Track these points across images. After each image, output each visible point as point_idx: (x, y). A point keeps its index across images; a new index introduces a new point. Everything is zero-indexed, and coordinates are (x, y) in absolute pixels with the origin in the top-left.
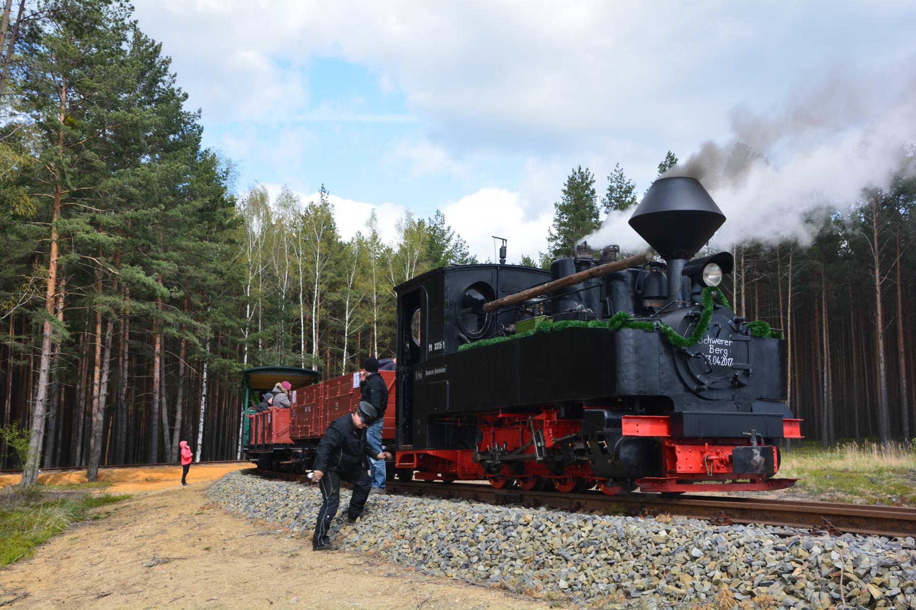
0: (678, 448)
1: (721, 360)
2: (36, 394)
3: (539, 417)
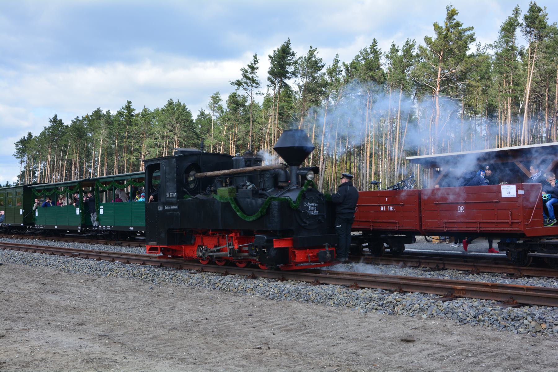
0: (297, 252)
1: (313, 212)
2: (467, 272)
3: (231, 235)
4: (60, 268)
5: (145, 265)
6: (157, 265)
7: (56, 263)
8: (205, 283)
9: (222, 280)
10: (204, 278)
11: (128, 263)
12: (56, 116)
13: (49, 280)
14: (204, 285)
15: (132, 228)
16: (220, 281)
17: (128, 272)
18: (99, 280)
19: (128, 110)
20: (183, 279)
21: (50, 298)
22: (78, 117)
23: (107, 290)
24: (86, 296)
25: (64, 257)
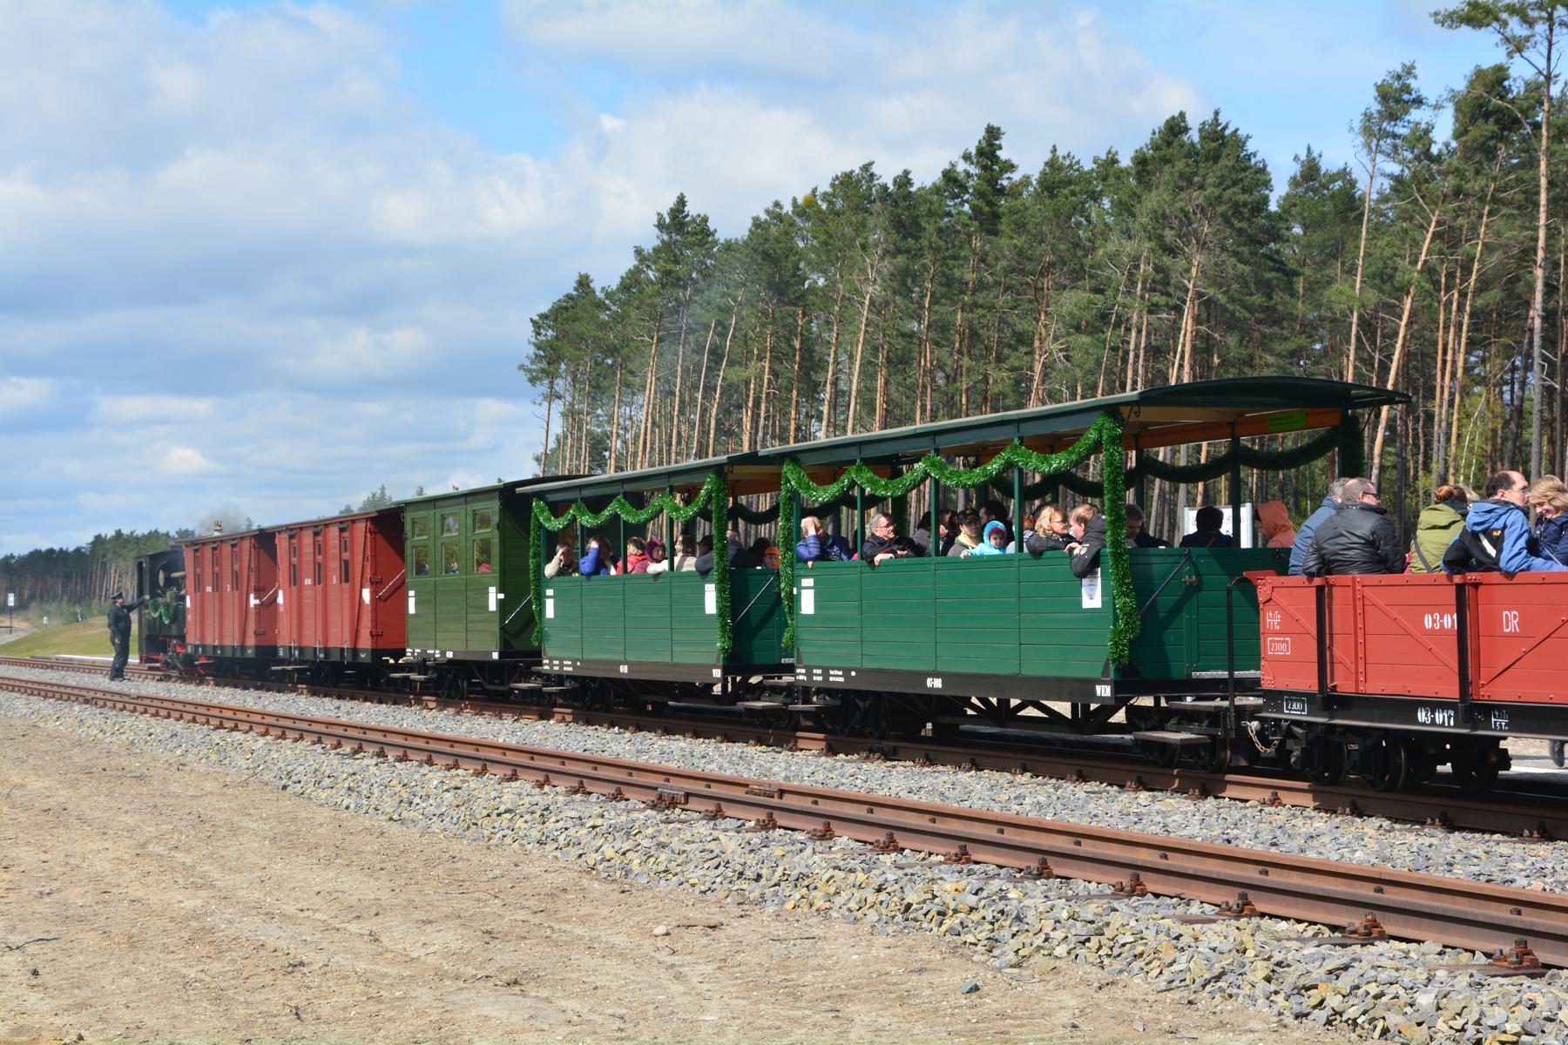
4: (592, 858)
5: (968, 861)
6: (1023, 865)
7: (584, 831)
8: (1250, 977)
9: (1346, 968)
10: (1250, 953)
11: (890, 846)
12: (681, 202)
13: (522, 915)
14: (1247, 990)
15: (937, 683)
16: (1334, 973)
17: (883, 896)
18: (737, 928)
19: (985, 168)
20: (1139, 949)
21: (485, 1011)
22: (777, 204)
23: (757, 987)
24: (651, 1014)
25: (622, 804)
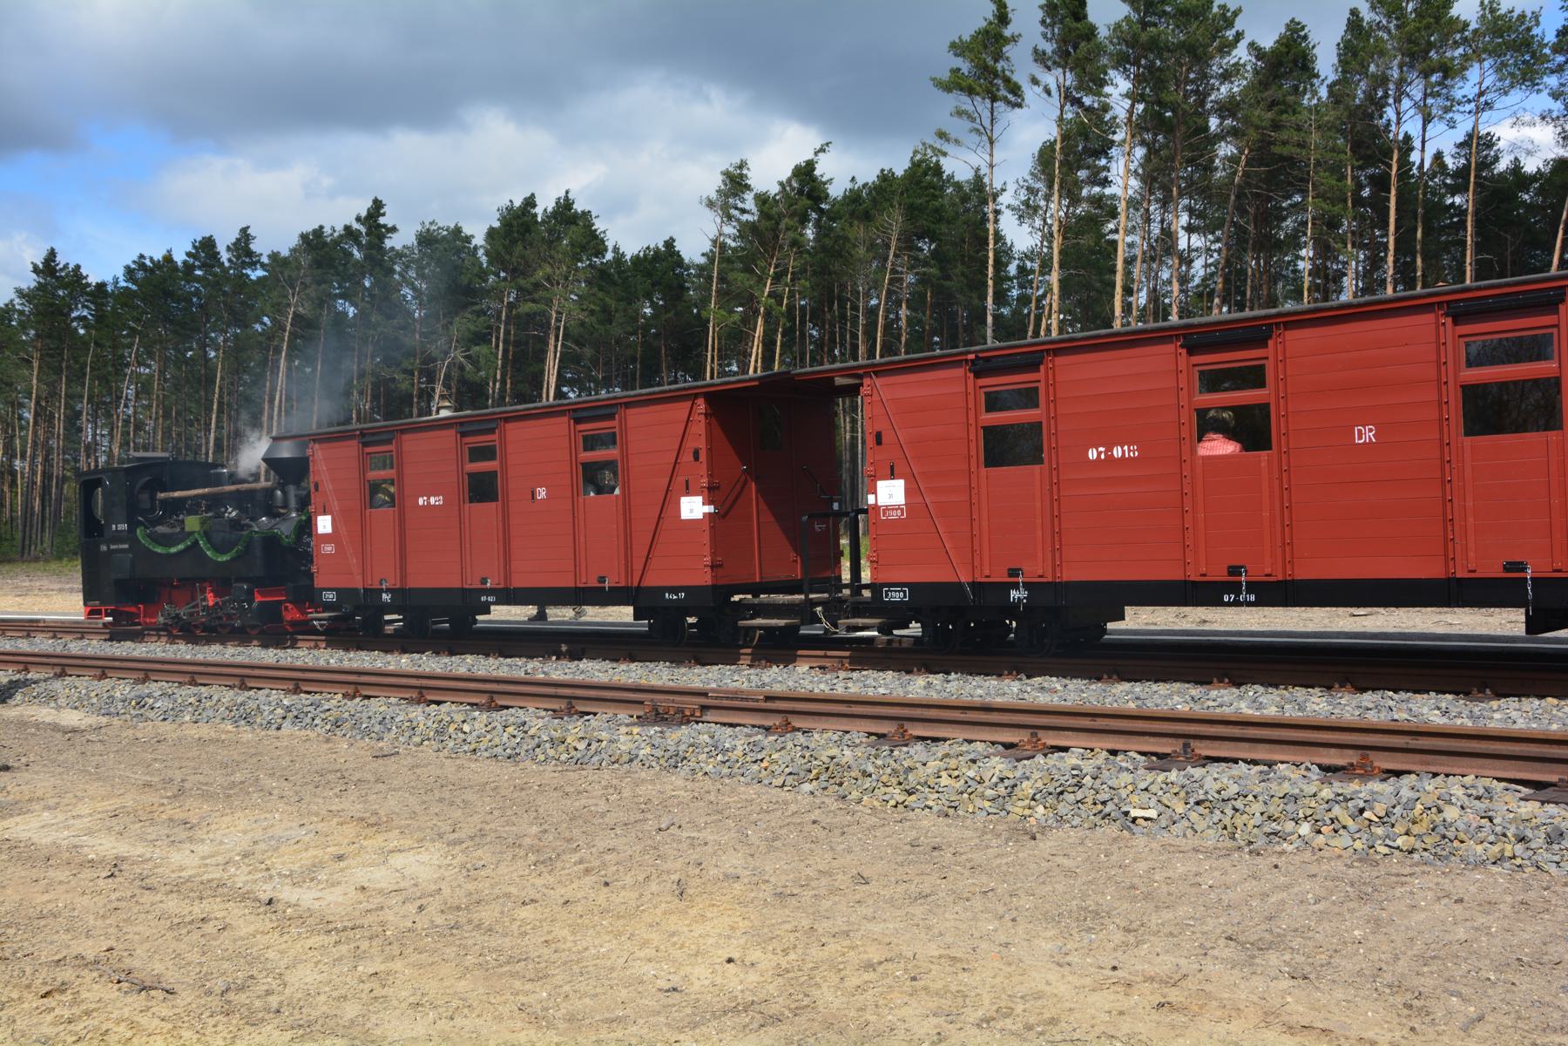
12: (52, 254)
22: (142, 256)
